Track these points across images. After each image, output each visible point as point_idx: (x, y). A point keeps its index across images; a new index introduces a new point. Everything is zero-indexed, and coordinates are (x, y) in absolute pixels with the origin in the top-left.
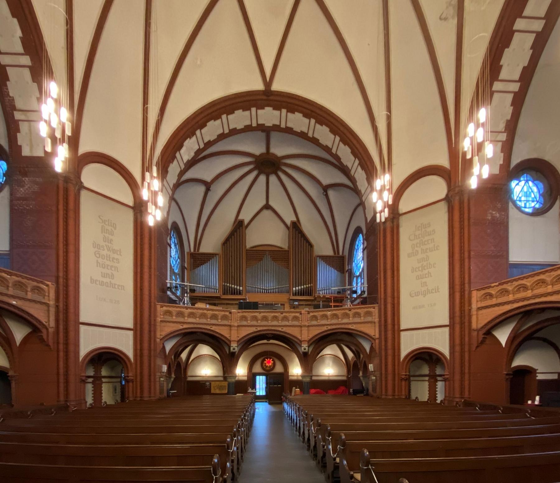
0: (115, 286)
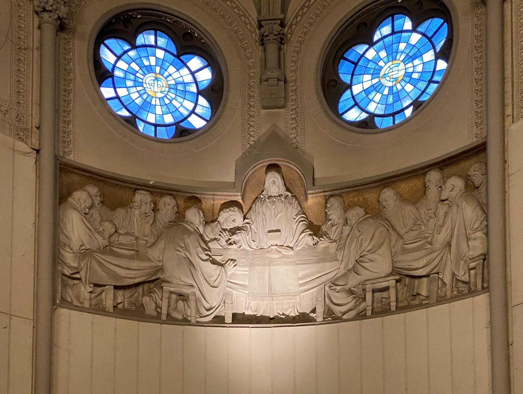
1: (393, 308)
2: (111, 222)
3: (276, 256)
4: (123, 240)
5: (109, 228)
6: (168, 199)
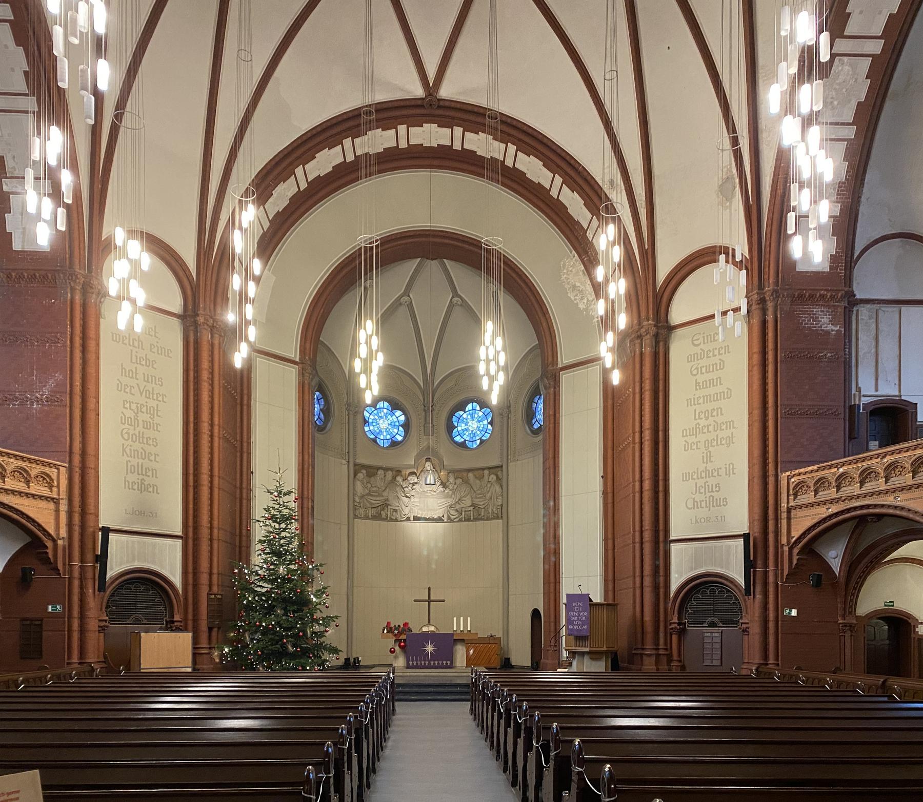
0: (157, 426)
4: (374, 489)
6: (390, 472)
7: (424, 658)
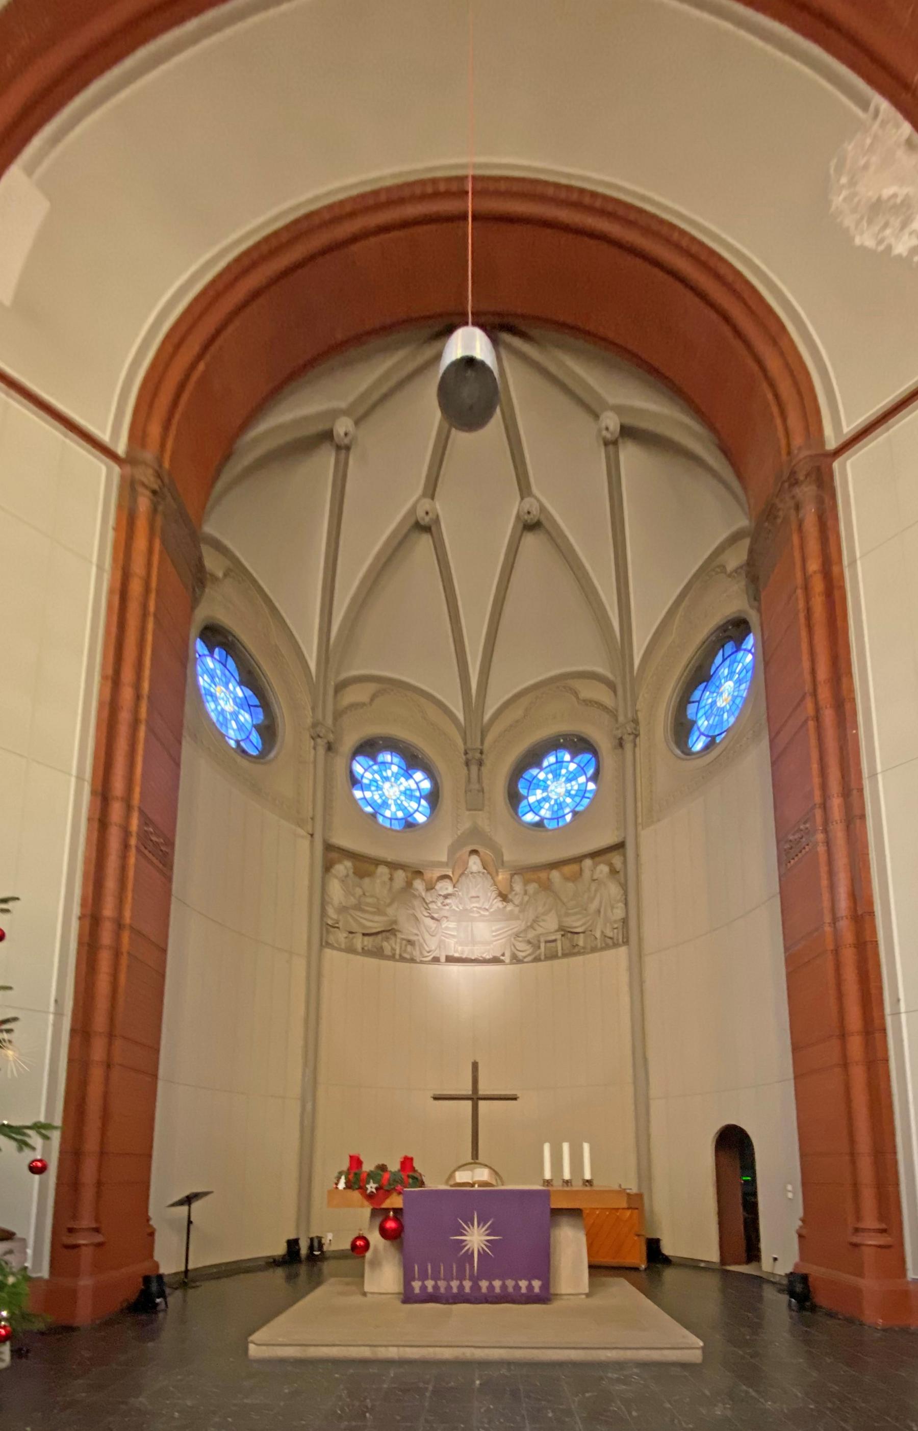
1: (560, 954)
2: (361, 887)
3: (477, 915)
4: (369, 900)
5: (359, 891)
7: (461, 1270)
